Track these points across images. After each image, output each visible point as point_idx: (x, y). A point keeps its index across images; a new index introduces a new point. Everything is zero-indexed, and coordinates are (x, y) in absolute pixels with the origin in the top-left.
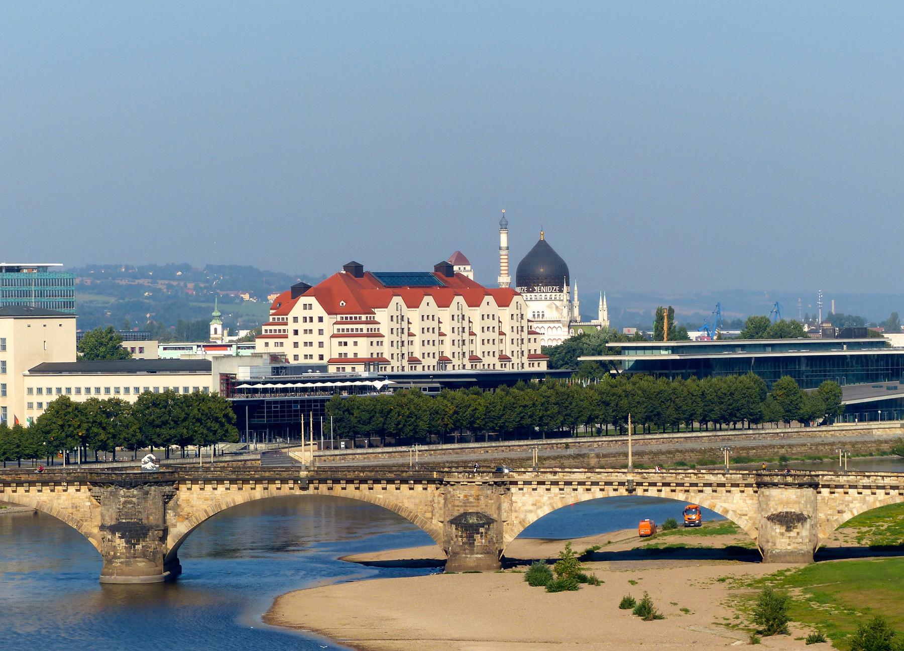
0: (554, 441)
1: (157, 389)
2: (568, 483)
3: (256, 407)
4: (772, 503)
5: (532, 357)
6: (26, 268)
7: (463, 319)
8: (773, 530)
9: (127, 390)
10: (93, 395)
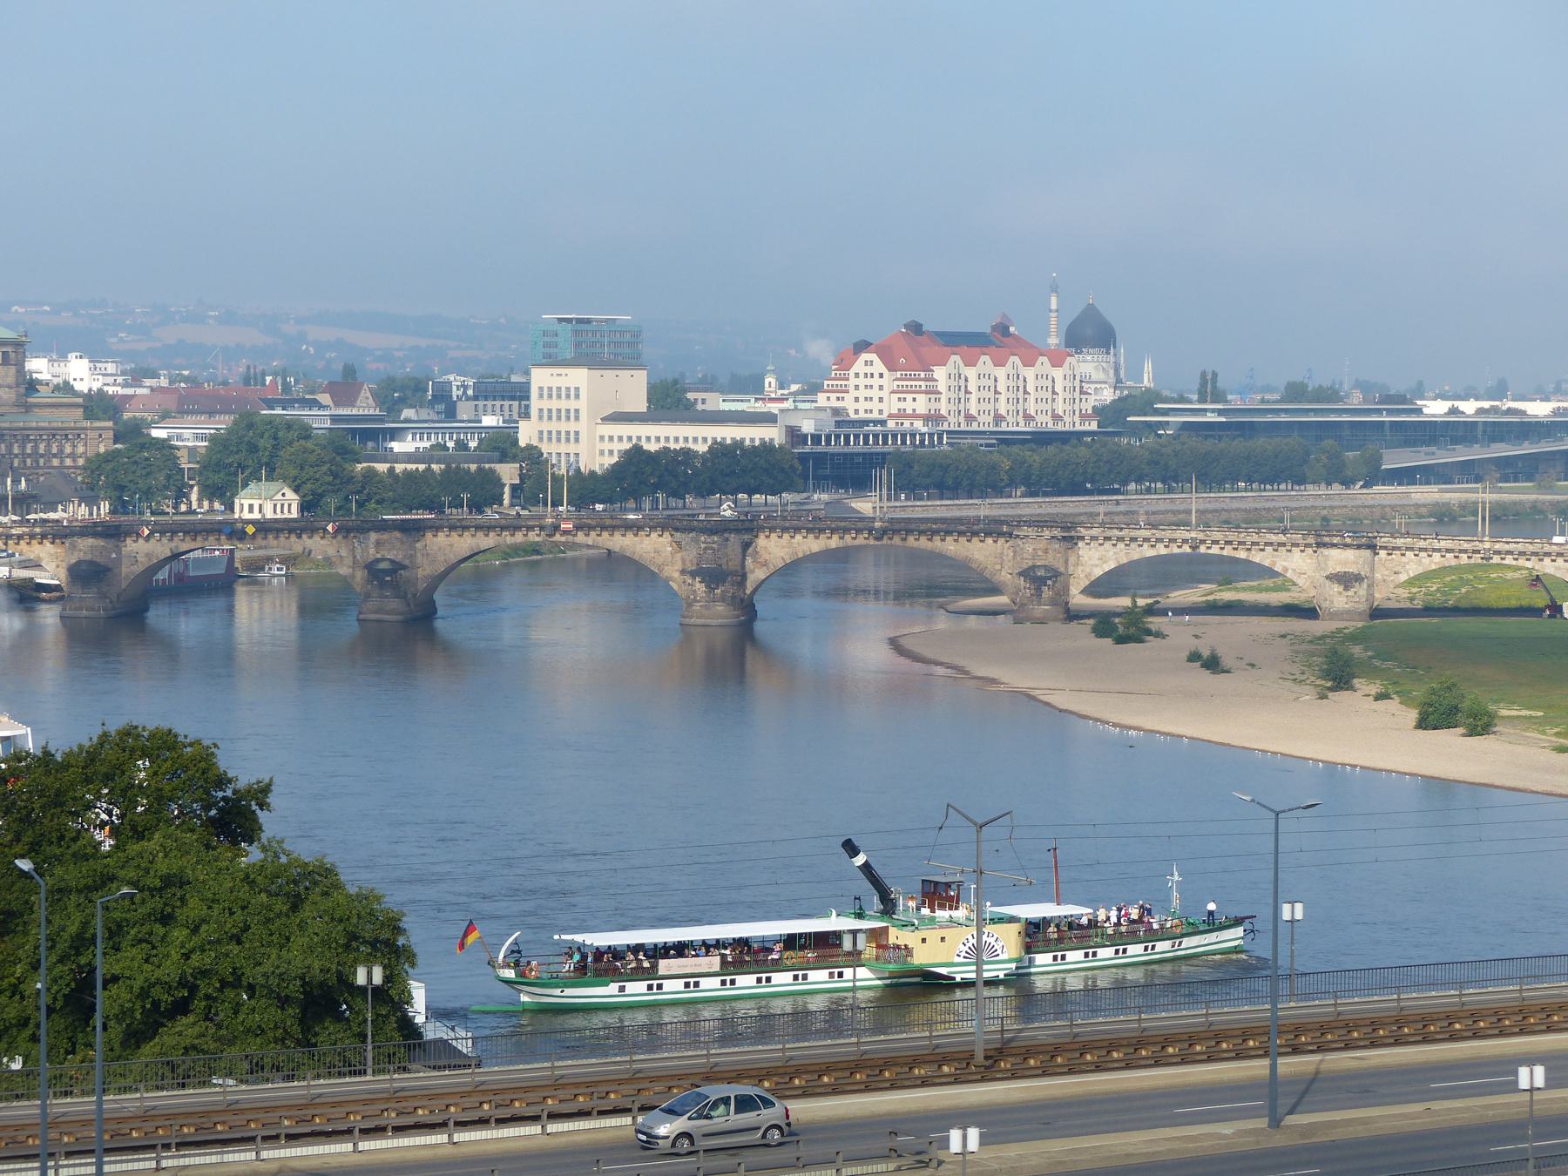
0: (1105, 498)
1: (724, 439)
2: (1133, 539)
3: (820, 459)
4: (1330, 563)
5: (1084, 417)
6: (597, 321)
7: (1018, 378)
8: (1332, 589)
9: (695, 440)
10: (691, 445)
